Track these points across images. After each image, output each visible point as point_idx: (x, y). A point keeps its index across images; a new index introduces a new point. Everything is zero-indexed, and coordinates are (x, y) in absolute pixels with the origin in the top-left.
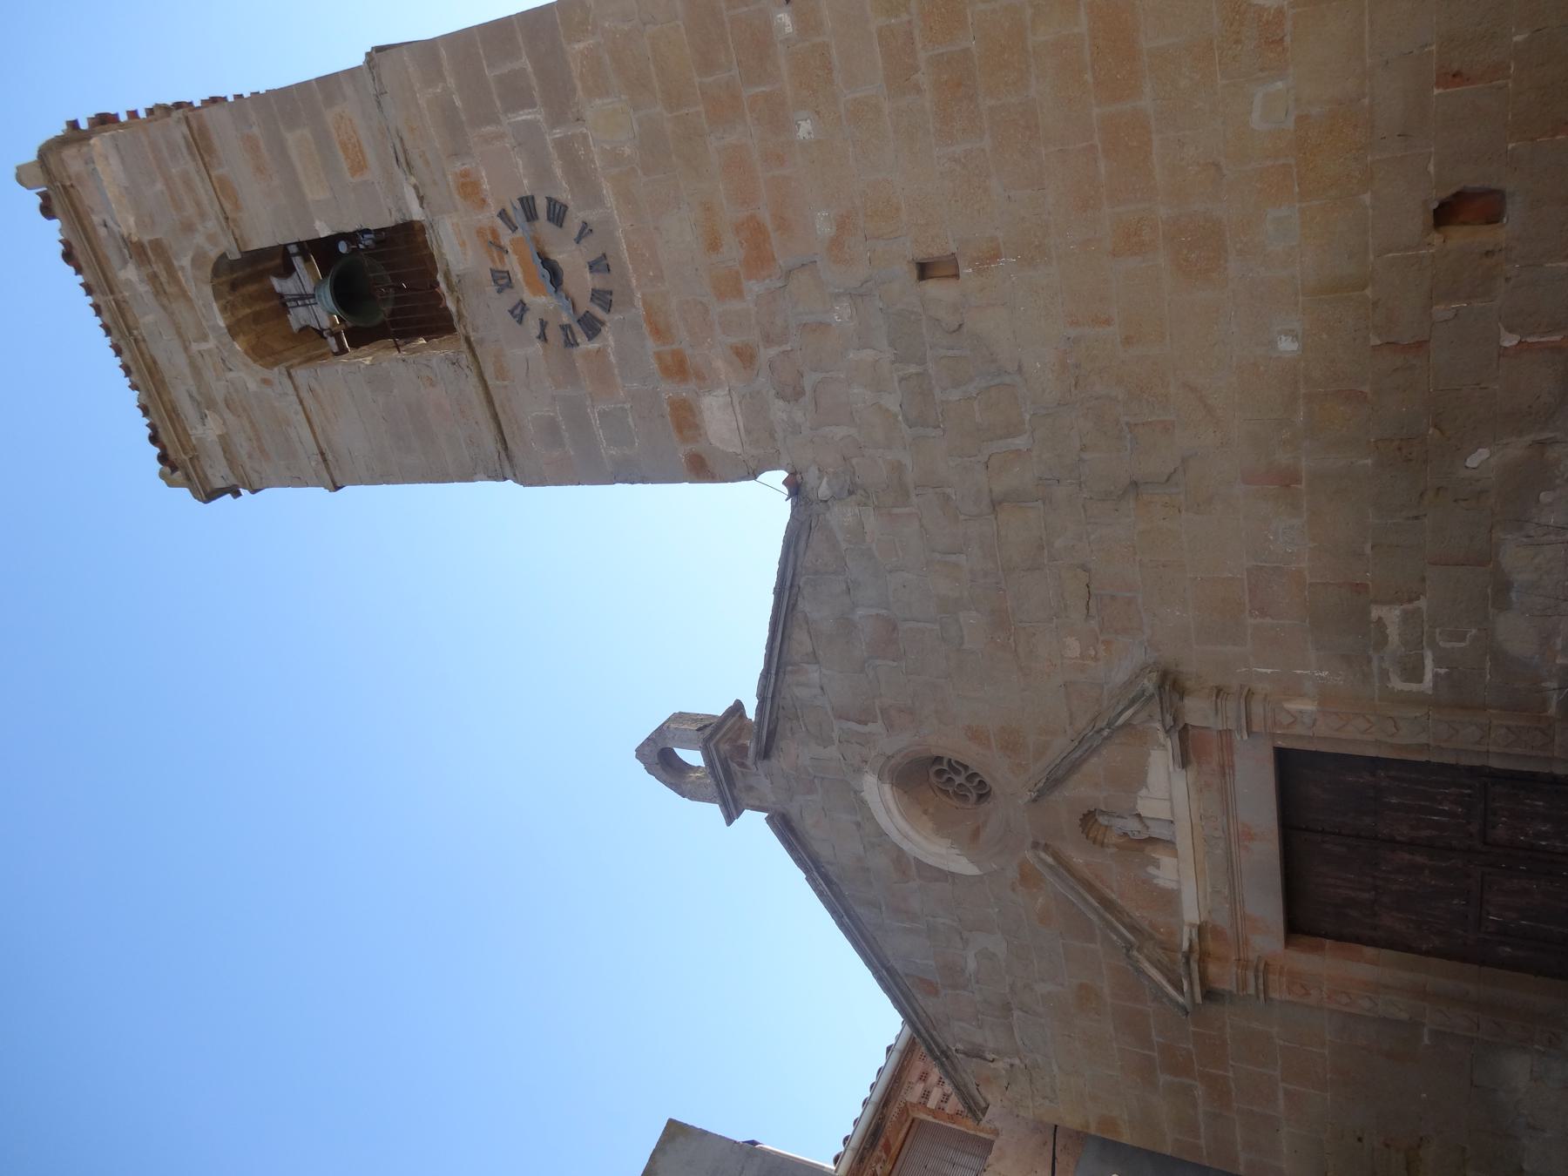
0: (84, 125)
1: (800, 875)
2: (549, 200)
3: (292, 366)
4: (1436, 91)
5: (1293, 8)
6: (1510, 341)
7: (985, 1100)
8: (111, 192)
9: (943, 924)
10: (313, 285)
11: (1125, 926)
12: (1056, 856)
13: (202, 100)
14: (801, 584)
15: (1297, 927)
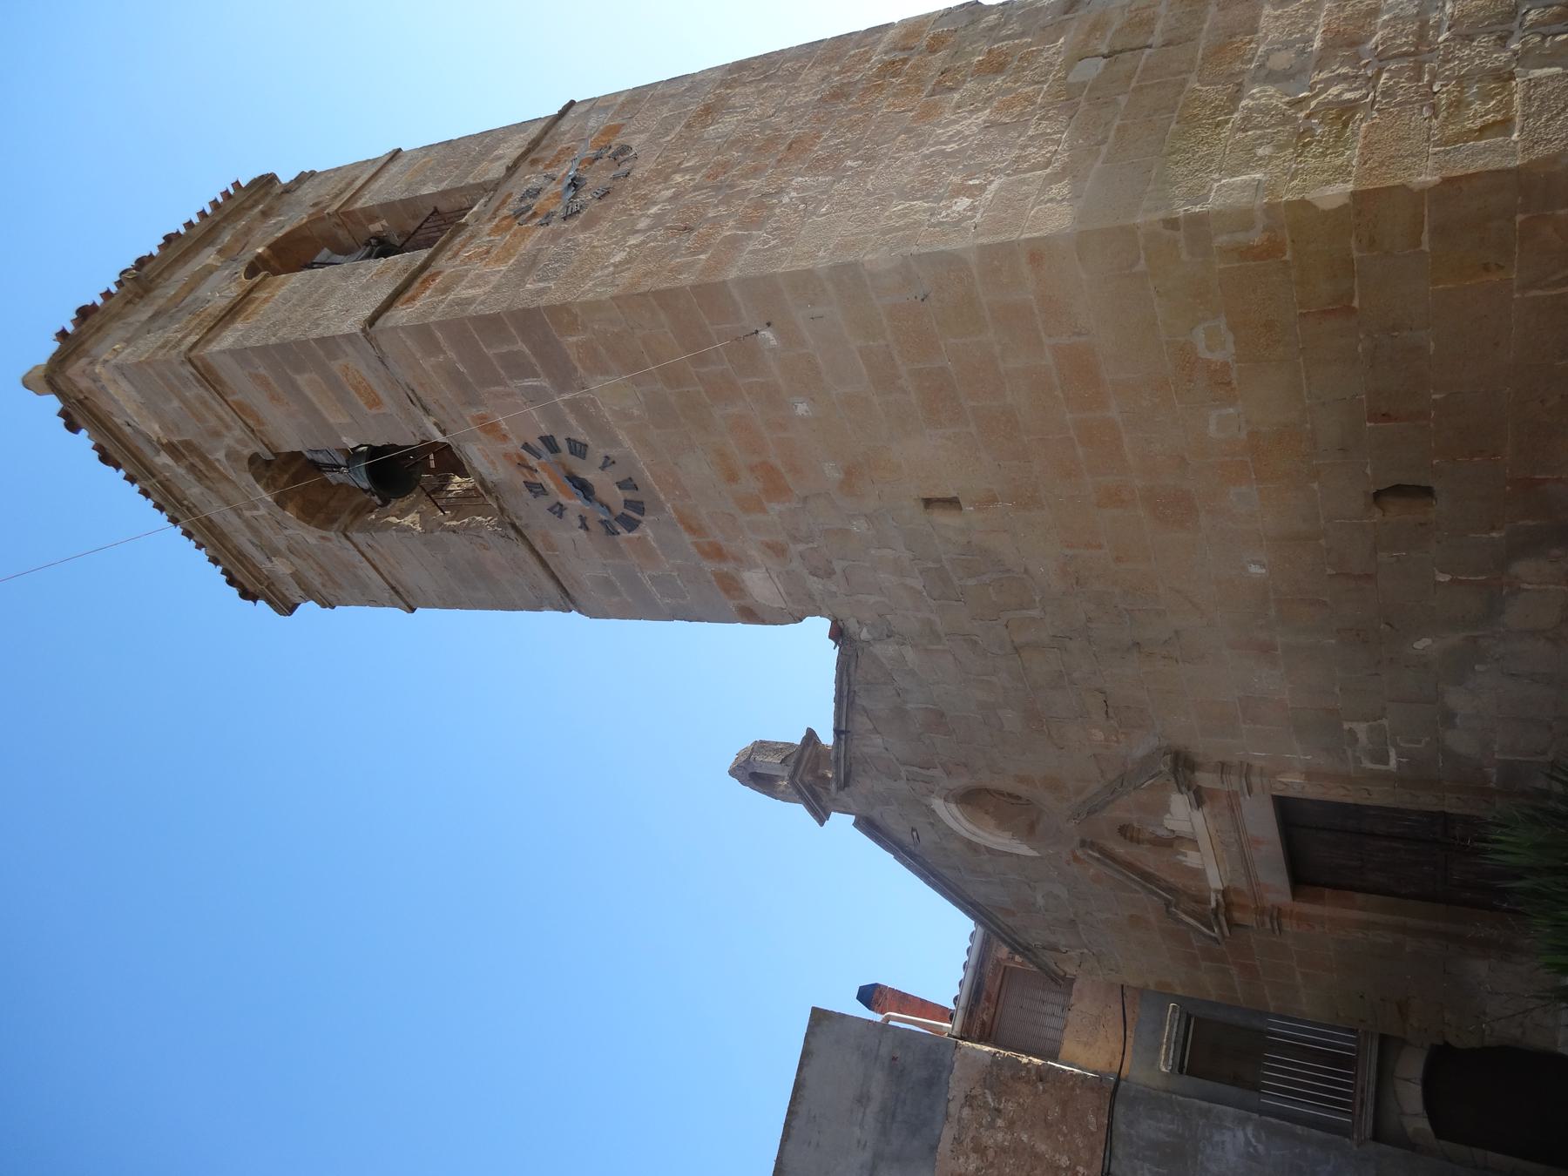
0: (70, 328)
2: (568, 440)
3: (346, 528)
4: (1368, 424)
5: (1237, 362)
6: (1444, 578)
7: (1064, 971)
8: (130, 408)
9: (1014, 879)
10: (344, 459)
13: (159, 246)
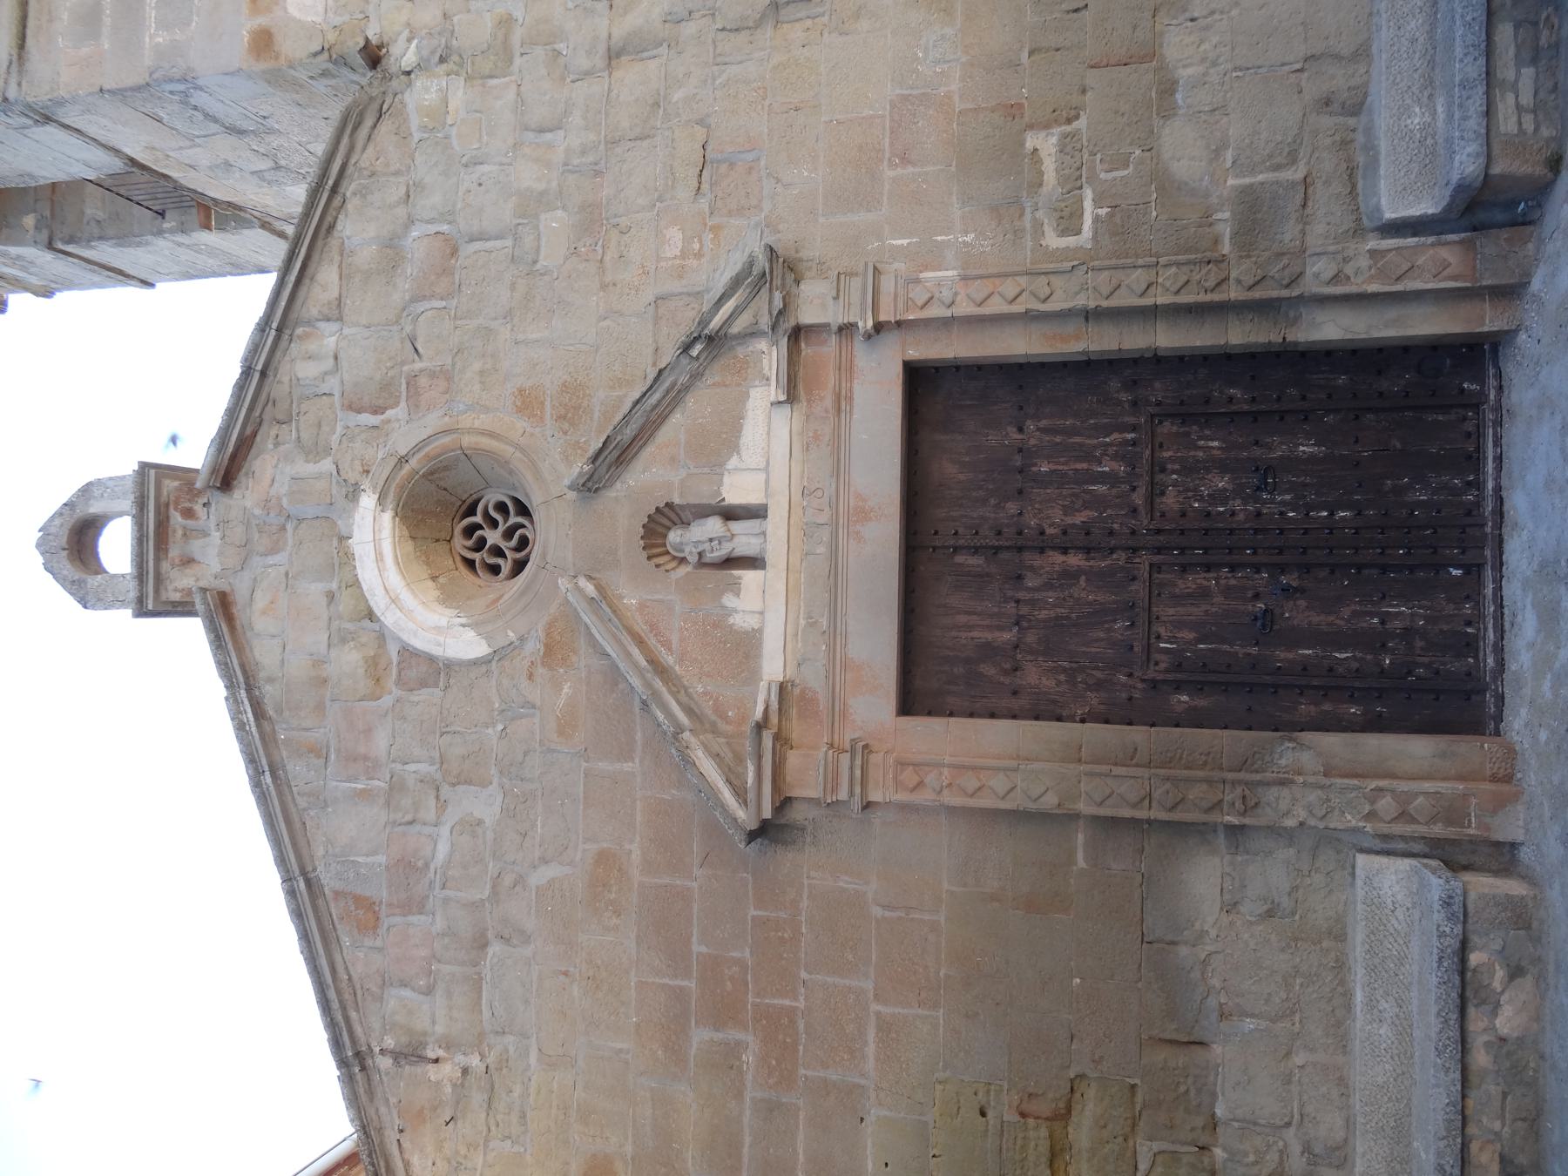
1: (219, 689)
12: (599, 588)
14: (348, 194)
15: (908, 704)
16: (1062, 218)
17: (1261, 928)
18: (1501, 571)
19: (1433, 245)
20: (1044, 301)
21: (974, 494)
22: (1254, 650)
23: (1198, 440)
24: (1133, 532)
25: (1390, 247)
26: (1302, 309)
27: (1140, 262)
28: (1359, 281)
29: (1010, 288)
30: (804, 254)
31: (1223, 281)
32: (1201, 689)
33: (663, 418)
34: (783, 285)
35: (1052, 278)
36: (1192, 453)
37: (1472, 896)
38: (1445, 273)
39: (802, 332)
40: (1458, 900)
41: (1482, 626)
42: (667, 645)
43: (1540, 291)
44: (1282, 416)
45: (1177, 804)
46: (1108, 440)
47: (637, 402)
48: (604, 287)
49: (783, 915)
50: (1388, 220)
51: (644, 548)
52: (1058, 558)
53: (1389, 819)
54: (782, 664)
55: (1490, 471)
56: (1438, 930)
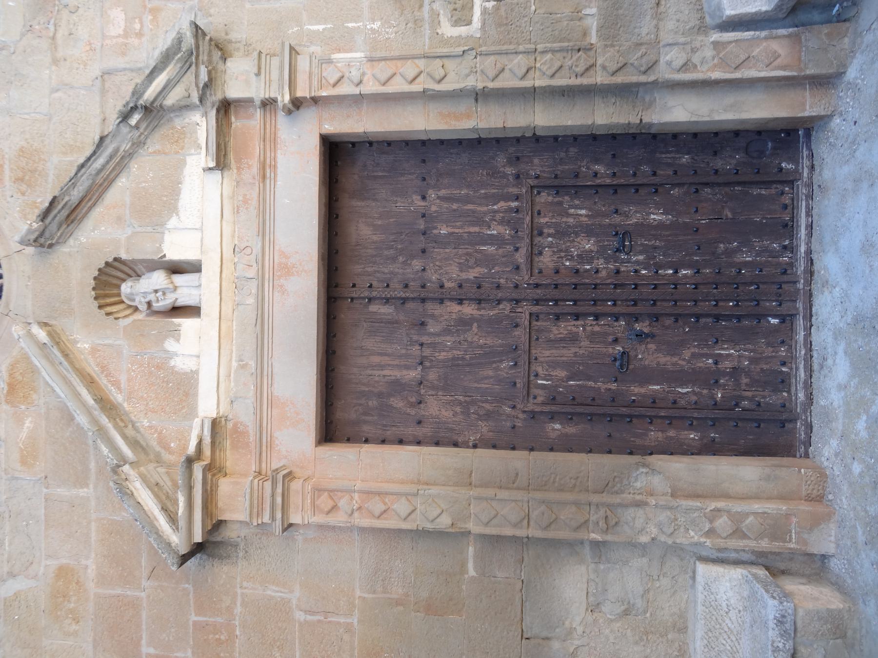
11: (125, 437)
16: (455, 10)
17: (619, 624)
18: (810, 321)
19: (766, 38)
20: (440, 82)
21: (386, 253)
22: (614, 386)
23: (569, 209)
24: (516, 286)
25: (731, 39)
26: (656, 95)
27: (521, 48)
28: (704, 70)
29: (409, 69)
30: (233, 36)
31: (591, 66)
32: (571, 419)
33: (109, 182)
34: (210, 61)
35: (447, 62)
36: (564, 219)
37: (801, 613)
38: (776, 63)
39: (232, 107)
40: (789, 619)
41: (794, 366)
42: (117, 384)
43: (856, 78)
44: (637, 188)
45: (551, 523)
46: (495, 207)
47: (82, 166)
48: (55, 62)
49: (219, 620)
50: (729, 17)
51: (96, 298)
52: (455, 307)
53: (725, 535)
54: (215, 402)
55: (803, 237)
56: (772, 645)
